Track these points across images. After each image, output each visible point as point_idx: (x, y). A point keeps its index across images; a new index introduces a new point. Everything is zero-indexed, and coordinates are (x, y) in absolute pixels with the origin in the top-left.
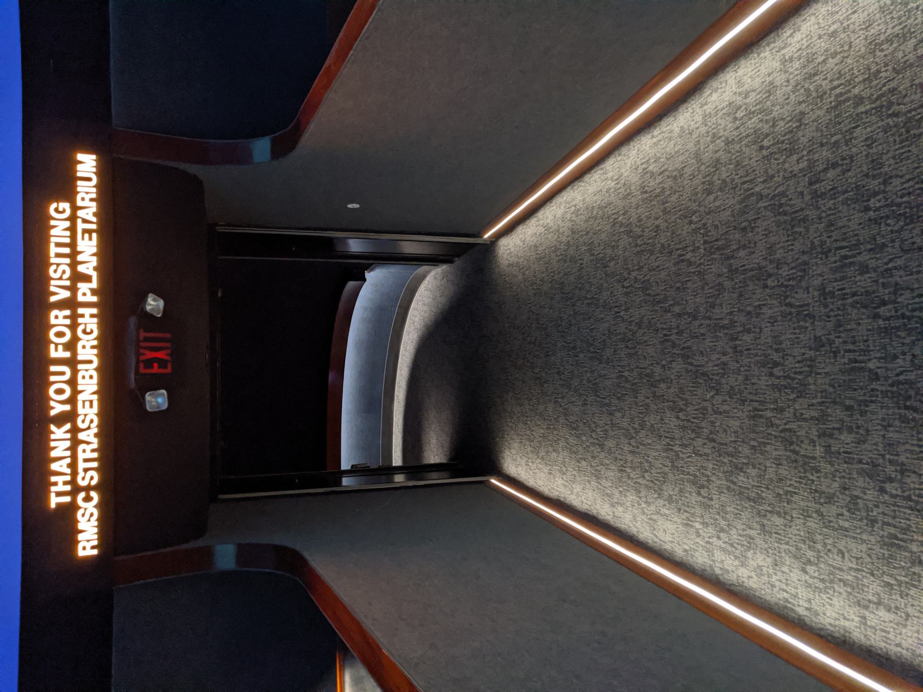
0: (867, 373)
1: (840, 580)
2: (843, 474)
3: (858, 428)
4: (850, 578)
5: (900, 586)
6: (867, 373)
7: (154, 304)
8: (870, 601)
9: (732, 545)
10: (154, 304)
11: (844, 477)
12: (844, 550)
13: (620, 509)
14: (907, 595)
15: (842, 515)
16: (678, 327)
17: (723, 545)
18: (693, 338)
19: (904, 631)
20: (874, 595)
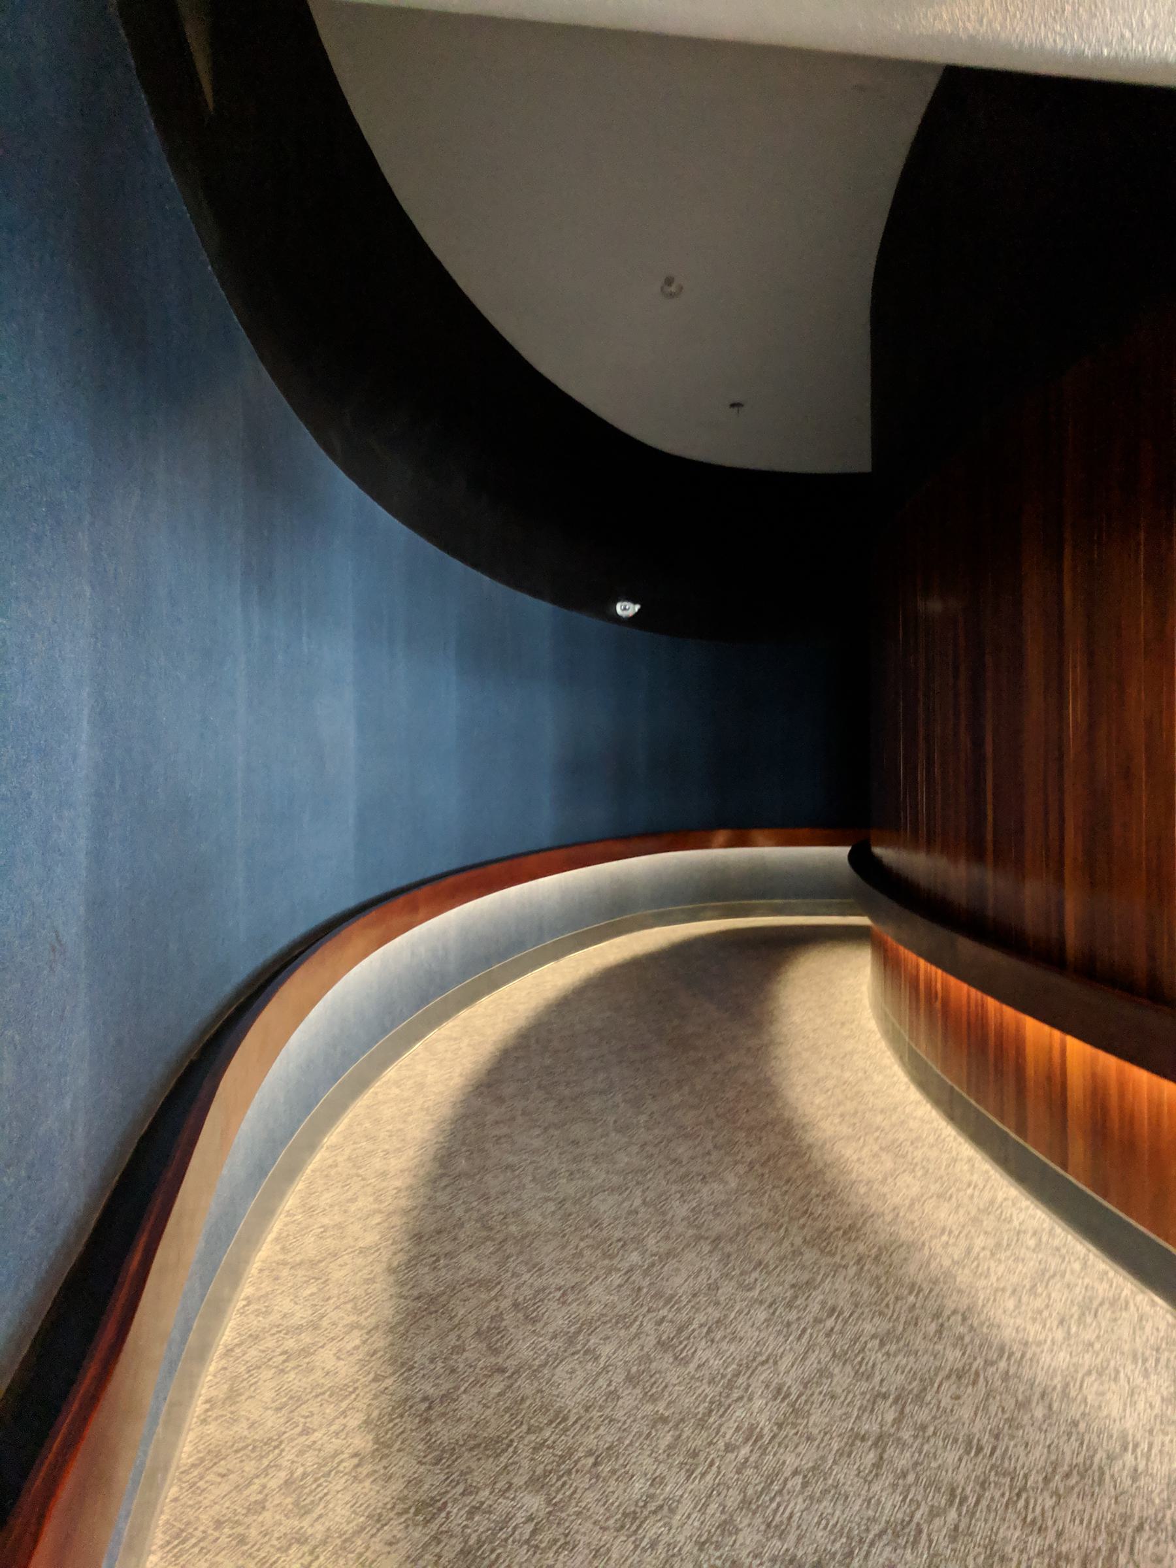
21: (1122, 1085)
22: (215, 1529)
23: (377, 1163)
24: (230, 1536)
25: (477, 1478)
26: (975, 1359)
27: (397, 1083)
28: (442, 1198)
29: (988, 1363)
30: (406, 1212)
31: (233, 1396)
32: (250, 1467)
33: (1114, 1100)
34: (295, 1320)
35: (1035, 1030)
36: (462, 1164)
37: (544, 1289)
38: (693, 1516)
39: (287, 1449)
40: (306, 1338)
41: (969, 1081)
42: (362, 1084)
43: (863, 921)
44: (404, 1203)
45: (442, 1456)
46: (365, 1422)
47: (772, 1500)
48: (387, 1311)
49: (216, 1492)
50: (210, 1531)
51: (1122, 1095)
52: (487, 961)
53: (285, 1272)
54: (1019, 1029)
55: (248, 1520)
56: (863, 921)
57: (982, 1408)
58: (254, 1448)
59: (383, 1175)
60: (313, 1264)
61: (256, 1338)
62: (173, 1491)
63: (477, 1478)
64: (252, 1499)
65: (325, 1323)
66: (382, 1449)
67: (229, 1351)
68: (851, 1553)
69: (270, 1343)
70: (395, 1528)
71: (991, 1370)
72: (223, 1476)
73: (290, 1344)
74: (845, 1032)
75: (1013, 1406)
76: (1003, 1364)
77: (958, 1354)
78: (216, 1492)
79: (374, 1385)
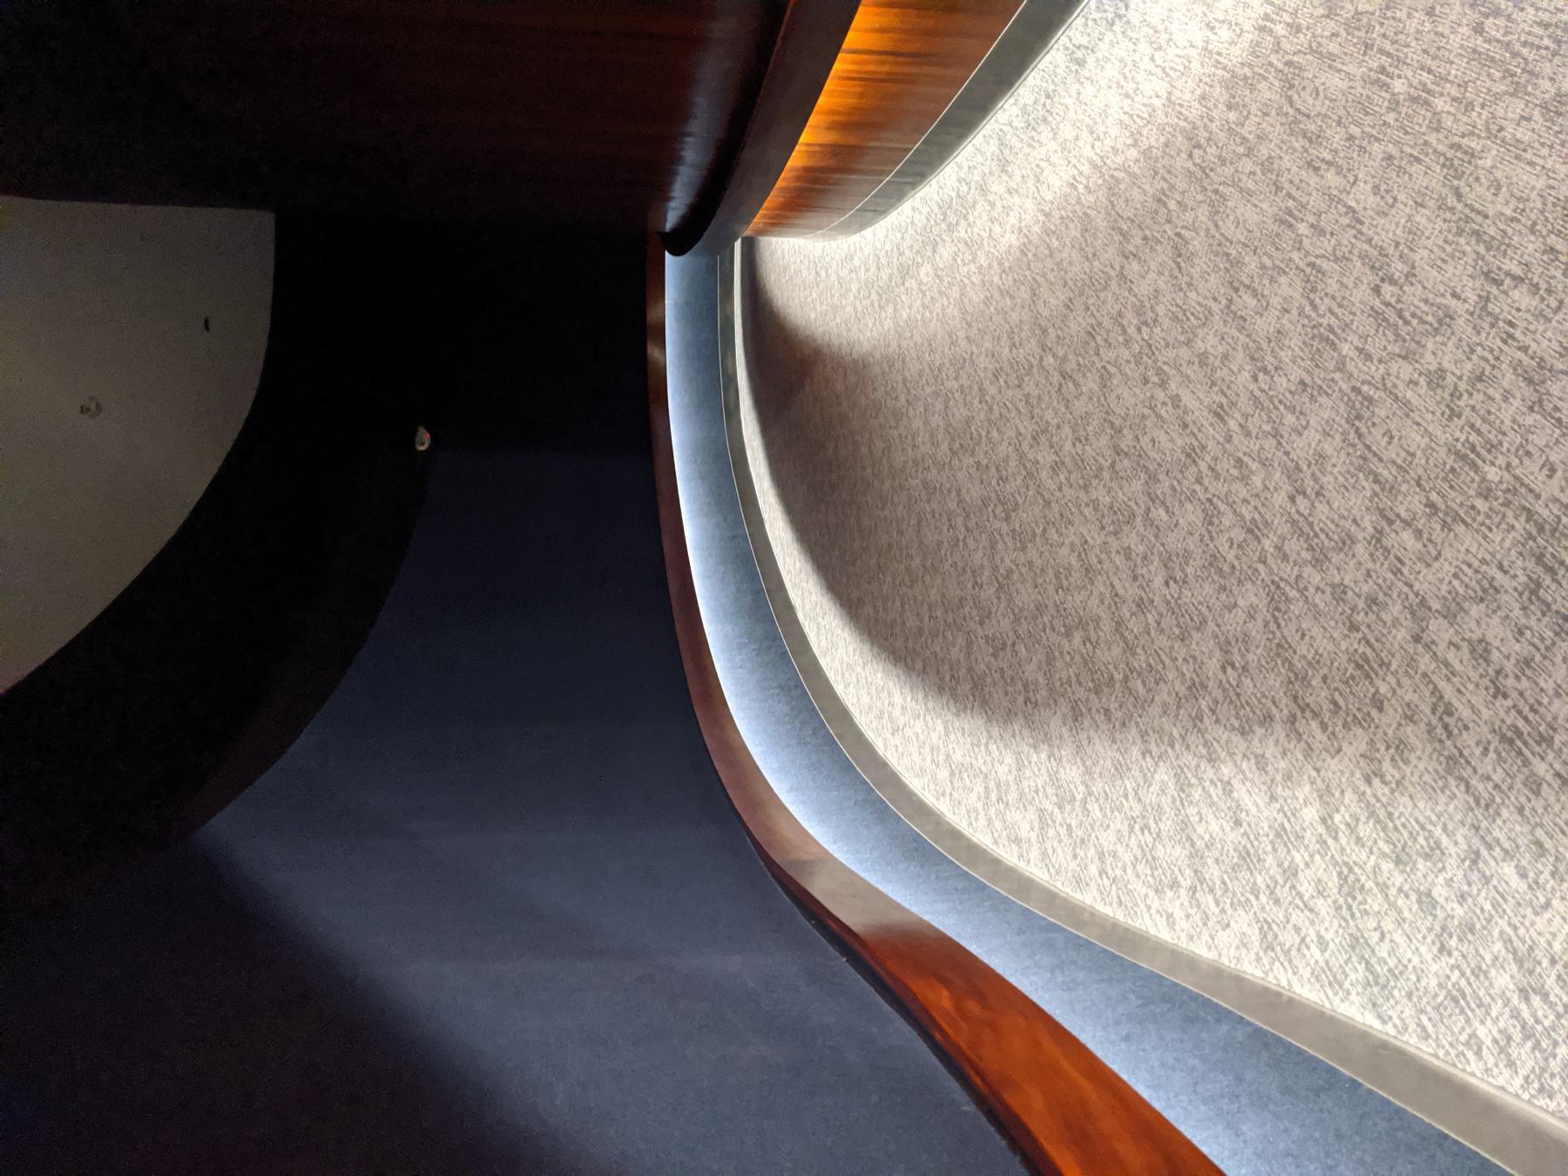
0: (1429, 115)
1: (1371, 472)
2: (1487, 354)
3: (1387, 191)
4: (1385, 472)
5: (1447, 514)
6: (1429, 115)
7: (423, 441)
8: (1398, 516)
9: (1271, 399)
10: (423, 441)
11: (1487, 361)
12: (1395, 433)
13: (1135, 265)
14: (1450, 530)
15: (1417, 384)
16: (1463, 86)
17: (1257, 393)
18: (1312, 51)
19: (1424, 571)
20: (1408, 510)
21: (832, 112)
22: (1450, 954)
23: (897, 712)
24: (1461, 940)
25: (1064, 674)
26: (1271, 64)
27: (847, 686)
28: (919, 665)
29: (1277, 48)
30: (926, 696)
31: (1017, 841)
32: (1375, 903)
33: (836, 118)
34: (981, 790)
35: (796, 160)
36: (899, 643)
37: (1294, 523)
38: (1418, 419)
39: (1354, 857)
40: (992, 784)
41: (872, 172)
42: (843, 715)
43: (738, 245)
44: (920, 697)
45: (1054, 696)
46: (1210, 761)
47: (1406, 323)
48: (980, 721)
49: (1061, 857)
50: (1452, 961)
51: (840, 113)
52: (757, 593)
53: (956, 795)
54: (781, 189)
55: (1440, 914)
56: (738, 245)
57: (1330, 61)
58: (1349, 894)
59: (903, 709)
60: (952, 774)
61: (990, 821)
62: (1059, 885)
63: (1064, 674)
64: (1415, 907)
65: (984, 769)
66: (1047, 739)
67: (996, 842)
68: (1477, 234)
69: (993, 810)
70: (1083, 736)
71: (1285, 45)
72: (1383, 935)
73: (994, 797)
74: (831, 271)
75: (1332, 24)
76: (1280, 30)
77: (1263, 86)
78: (1061, 857)
79: (1177, 746)
